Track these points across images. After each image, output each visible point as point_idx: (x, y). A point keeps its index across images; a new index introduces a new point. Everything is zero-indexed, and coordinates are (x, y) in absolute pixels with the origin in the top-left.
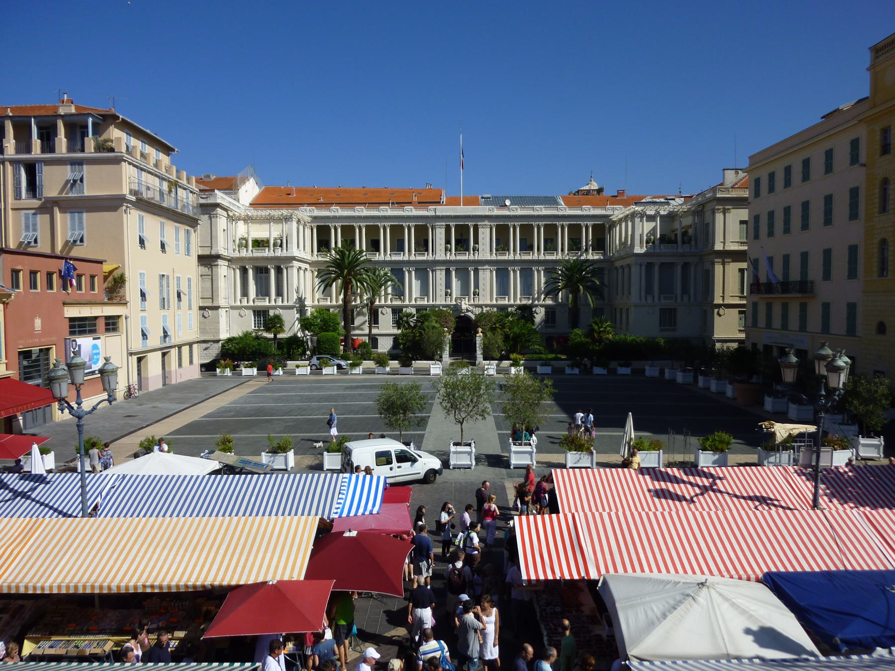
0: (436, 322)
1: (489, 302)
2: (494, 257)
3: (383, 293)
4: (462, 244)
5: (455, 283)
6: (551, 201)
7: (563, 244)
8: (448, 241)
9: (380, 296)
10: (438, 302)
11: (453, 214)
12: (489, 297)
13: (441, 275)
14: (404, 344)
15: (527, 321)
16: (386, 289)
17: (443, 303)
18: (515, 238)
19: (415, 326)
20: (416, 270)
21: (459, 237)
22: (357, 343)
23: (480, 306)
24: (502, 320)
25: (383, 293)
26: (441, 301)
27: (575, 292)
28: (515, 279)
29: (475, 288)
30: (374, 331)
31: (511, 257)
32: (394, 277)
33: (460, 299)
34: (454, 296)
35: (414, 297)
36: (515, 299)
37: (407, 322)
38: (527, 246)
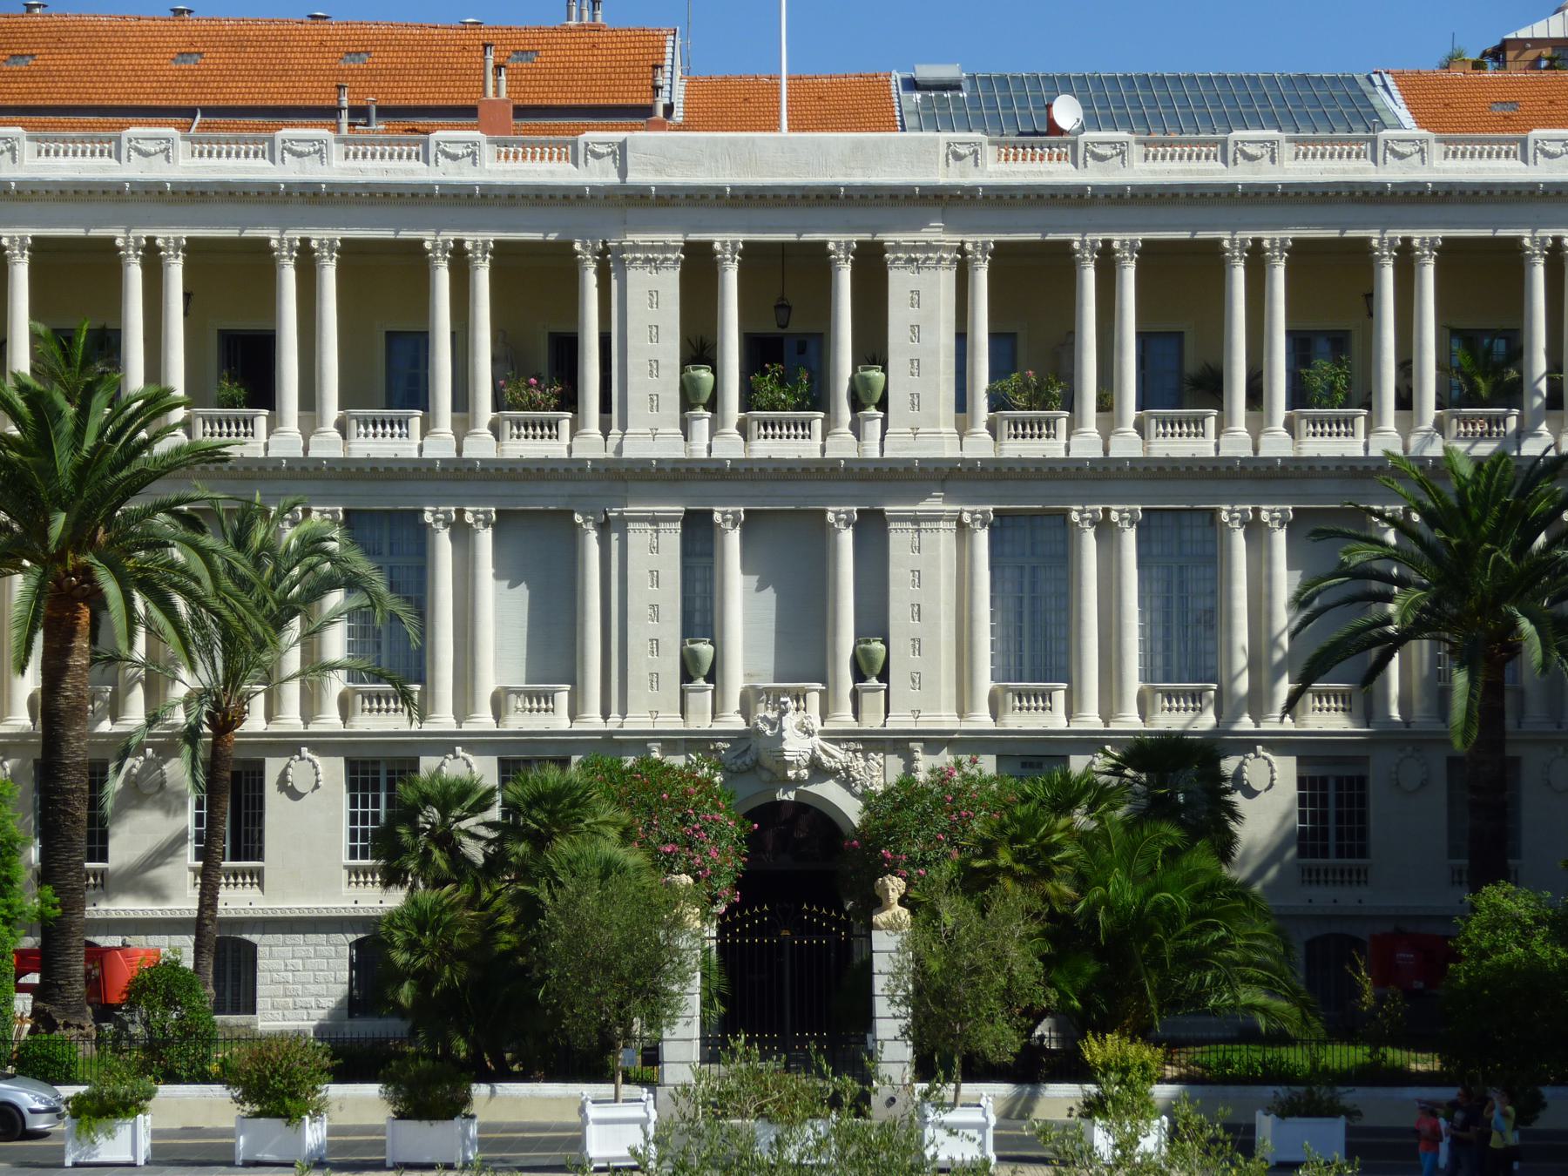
0: (626, 836)
1: (946, 719)
2: (980, 446)
3: (293, 661)
4: (786, 363)
5: (745, 606)
6: (1336, 106)
7: (1406, 367)
8: (699, 348)
9: (273, 682)
10: (638, 721)
11: (728, 177)
12: (947, 691)
13: (654, 553)
14: (424, 979)
15: (1195, 833)
16: (311, 639)
17: (670, 721)
18: (1109, 327)
19: (495, 864)
20: (504, 523)
21: (769, 327)
22: (122, 976)
23: (898, 744)
24: (1030, 825)
25: (293, 661)
26: (653, 709)
27: (1490, 655)
28: (1110, 581)
29: (861, 634)
30: (235, 901)
31: (1087, 445)
32: (362, 565)
33: (774, 696)
34: (736, 680)
35: (488, 682)
36: (1113, 697)
37: (446, 840)
38: (1183, 376)
